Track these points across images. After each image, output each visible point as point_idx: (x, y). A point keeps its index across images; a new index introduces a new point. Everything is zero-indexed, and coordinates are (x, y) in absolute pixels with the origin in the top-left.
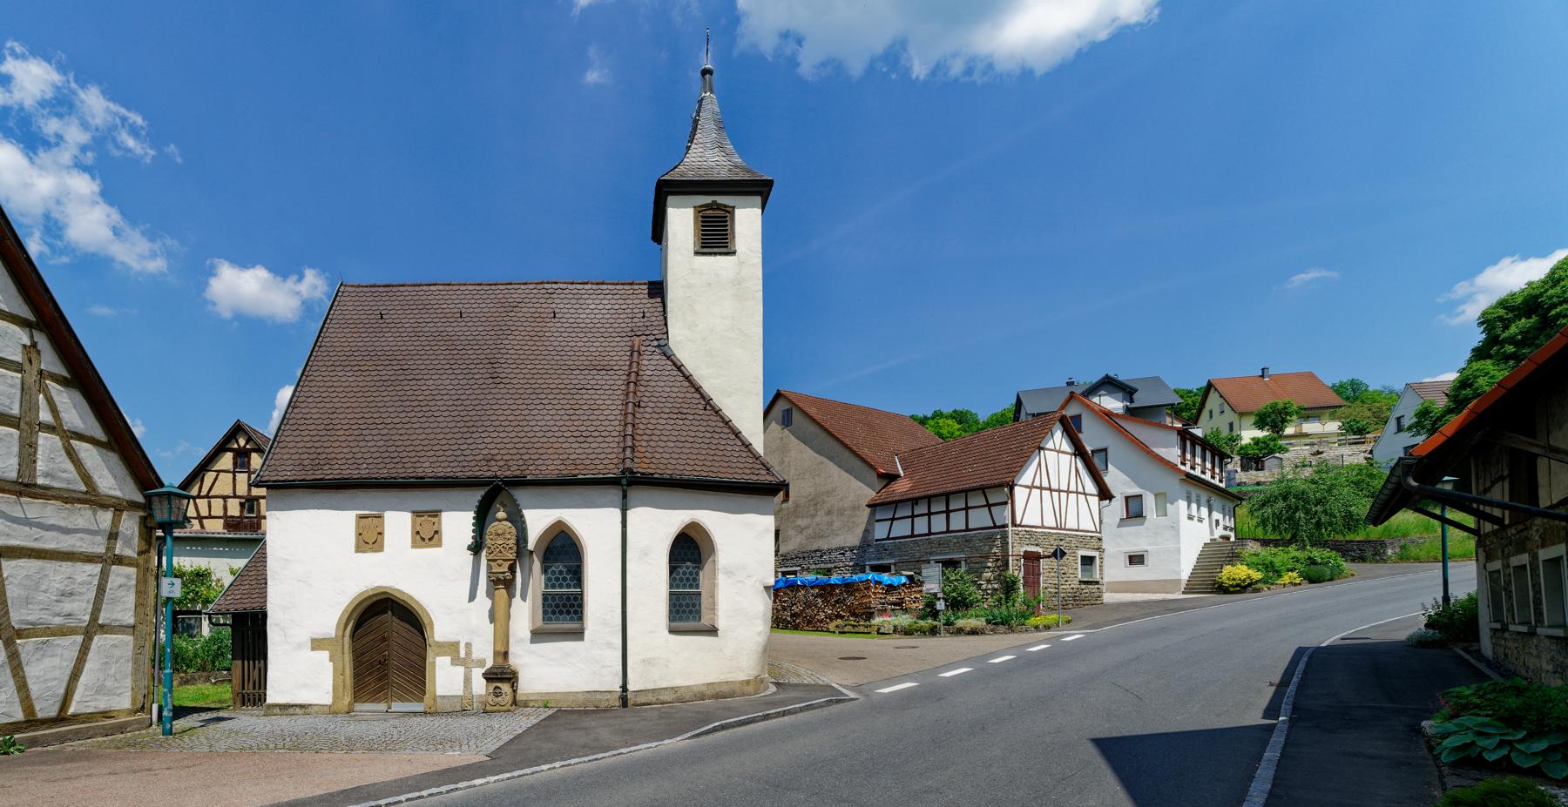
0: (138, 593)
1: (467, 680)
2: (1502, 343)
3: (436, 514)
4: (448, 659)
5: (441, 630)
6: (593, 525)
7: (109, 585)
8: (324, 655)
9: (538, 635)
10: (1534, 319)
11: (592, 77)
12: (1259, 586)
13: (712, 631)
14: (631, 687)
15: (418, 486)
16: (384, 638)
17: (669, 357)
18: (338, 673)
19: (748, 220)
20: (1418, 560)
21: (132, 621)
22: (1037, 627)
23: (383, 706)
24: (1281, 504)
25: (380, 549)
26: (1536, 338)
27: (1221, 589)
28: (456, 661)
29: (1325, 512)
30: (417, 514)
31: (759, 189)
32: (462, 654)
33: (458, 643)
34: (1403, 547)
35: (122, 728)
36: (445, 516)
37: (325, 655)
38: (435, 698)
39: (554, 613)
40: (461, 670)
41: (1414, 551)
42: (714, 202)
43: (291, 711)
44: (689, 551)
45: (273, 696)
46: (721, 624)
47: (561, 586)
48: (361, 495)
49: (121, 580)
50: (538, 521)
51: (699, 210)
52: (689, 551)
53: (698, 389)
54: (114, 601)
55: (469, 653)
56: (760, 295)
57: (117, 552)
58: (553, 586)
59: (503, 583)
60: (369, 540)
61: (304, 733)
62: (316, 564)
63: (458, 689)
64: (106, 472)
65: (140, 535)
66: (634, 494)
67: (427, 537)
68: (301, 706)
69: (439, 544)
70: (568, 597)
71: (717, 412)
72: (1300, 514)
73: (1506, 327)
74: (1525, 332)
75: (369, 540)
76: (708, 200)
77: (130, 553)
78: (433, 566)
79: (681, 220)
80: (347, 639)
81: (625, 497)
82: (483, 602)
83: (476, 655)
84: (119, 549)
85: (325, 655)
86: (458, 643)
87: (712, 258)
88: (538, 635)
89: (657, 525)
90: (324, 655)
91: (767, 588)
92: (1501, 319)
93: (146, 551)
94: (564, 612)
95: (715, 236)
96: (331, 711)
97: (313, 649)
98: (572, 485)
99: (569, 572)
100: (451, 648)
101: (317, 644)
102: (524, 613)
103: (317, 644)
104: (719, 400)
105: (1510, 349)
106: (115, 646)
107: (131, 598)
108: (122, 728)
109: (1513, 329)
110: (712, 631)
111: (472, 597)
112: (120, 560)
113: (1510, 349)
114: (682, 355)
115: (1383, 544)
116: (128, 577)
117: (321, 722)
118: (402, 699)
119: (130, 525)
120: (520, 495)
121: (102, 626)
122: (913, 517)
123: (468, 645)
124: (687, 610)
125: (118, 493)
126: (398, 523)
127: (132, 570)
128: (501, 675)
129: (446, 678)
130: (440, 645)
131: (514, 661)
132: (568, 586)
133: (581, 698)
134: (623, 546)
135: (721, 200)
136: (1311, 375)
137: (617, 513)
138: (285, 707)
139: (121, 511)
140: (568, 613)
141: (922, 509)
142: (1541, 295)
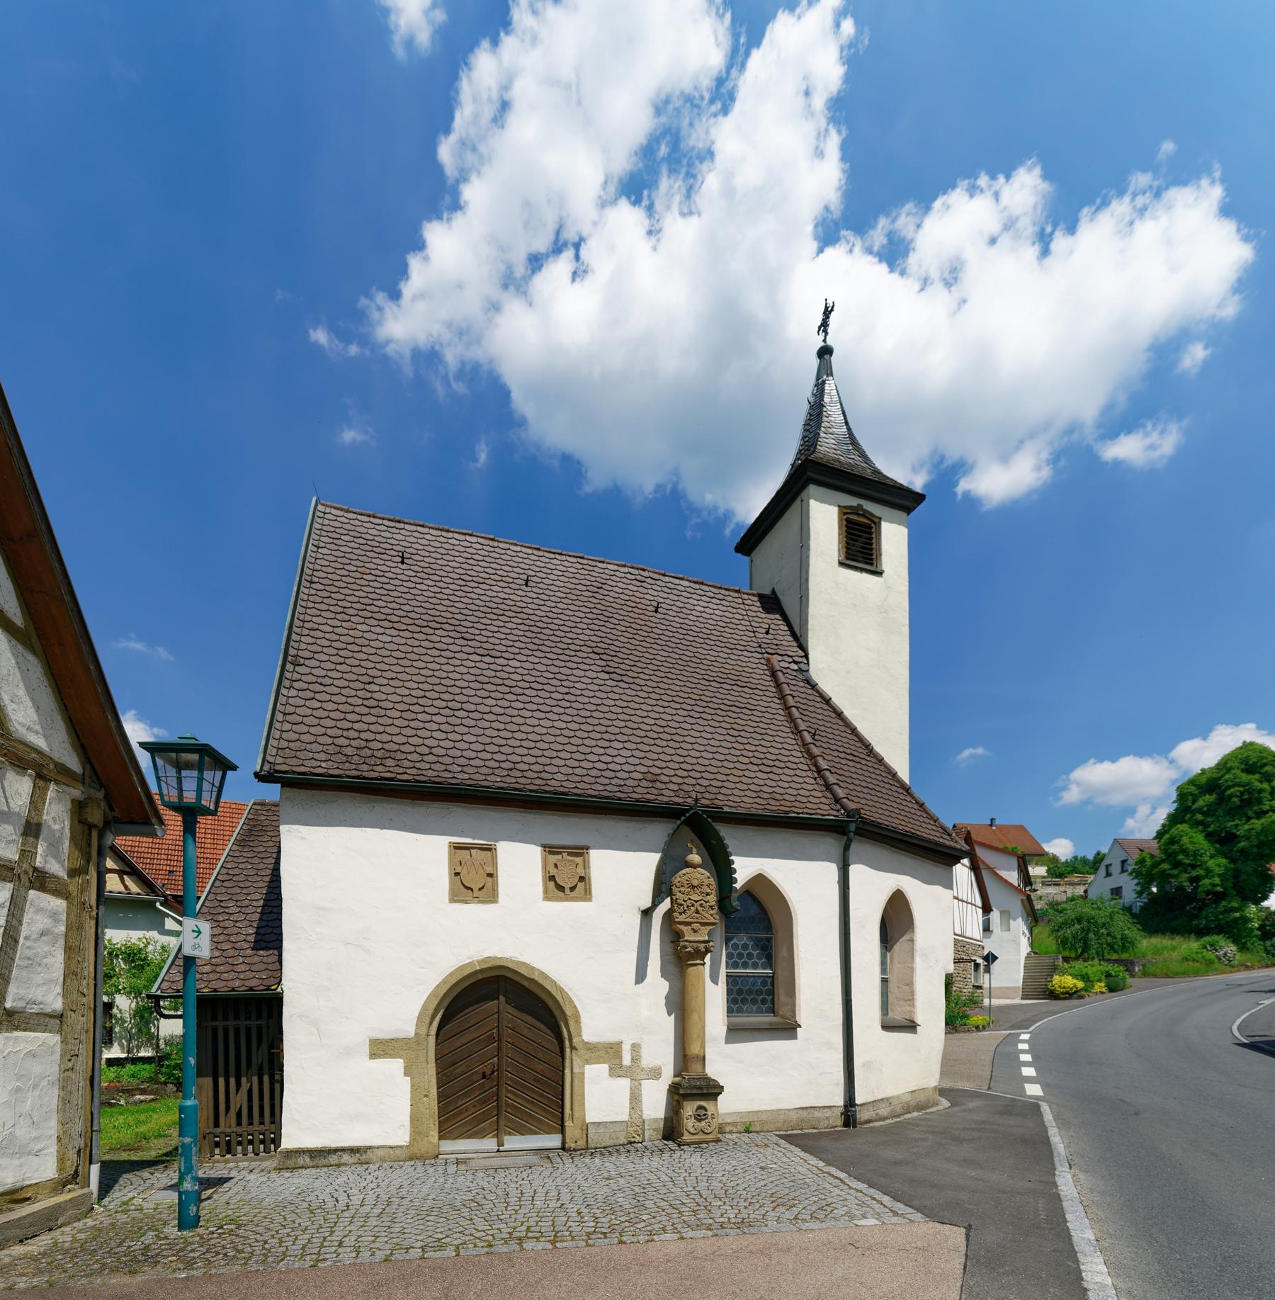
0: (68, 949)
1: (635, 1099)
2: (1194, 812)
3: (580, 851)
4: (605, 1067)
5: (592, 1024)
6: (804, 883)
7: (25, 930)
8: (396, 1065)
9: (736, 1033)
10: (1214, 796)
11: (349, 436)
12: (1083, 993)
14: (859, 1100)
15: (567, 809)
16: (497, 1043)
17: (813, 686)
18: (417, 1093)
19: (894, 538)
20: (1155, 976)
21: (58, 1005)
22: (977, 1028)
23: (489, 1144)
24: (1077, 926)
25: (493, 897)
26: (1216, 810)
27: (1052, 995)
28: (617, 1070)
29: (1109, 934)
30: (550, 849)
32: (627, 1060)
33: (619, 1044)
34: (1144, 966)
35: (48, 1221)
37: (397, 1065)
38: (585, 1128)
40: (625, 1083)
41: (1152, 969)
42: (860, 506)
43: (333, 1159)
45: (293, 1136)
47: (745, 965)
48: (458, 813)
49: (42, 922)
51: (844, 511)
52: (896, 921)
54: (32, 963)
55: (636, 1059)
56: (906, 630)
57: (39, 862)
59: (681, 958)
60: (475, 882)
62: (372, 925)
64: (21, 692)
65: (73, 838)
66: (857, 847)
67: (566, 883)
68: (353, 1151)
69: (587, 895)
70: (764, 978)
72: (1091, 935)
73: (1194, 802)
74: (1209, 806)
75: (475, 882)
77: (57, 868)
78: (587, 931)
80: (432, 1040)
81: (846, 848)
82: (658, 986)
83: (647, 1061)
84: (42, 858)
85: (397, 1065)
86: (619, 1044)
89: (873, 885)
90: (396, 1065)
92: (1191, 794)
93: (83, 871)
94: (764, 1005)
95: (860, 549)
96: (413, 1155)
97: (373, 1056)
98: (784, 825)
99: (756, 946)
100: (609, 1052)
101: (380, 1048)
102: (714, 999)
103: (380, 1048)
104: (878, 748)
105: (1200, 817)
106: (32, 1054)
107: (57, 960)
108: (48, 1221)
109: (1200, 803)
111: (640, 976)
112: (41, 881)
113: (1200, 817)
114: (826, 686)
115: (1132, 963)
116: (54, 915)
117: (400, 1177)
118: (522, 1131)
119: (57, 813)
121: (10, 1013)
123: (635, 1048)
125: (41, 743)
126: (519, 862)
127: (59, 904)
128: (693, 1088)
129: (601, 1098)
130: (591, 1047)
131: (715, 1069)
132: (755, 966)
133: (795, 1116)
135: (869, 506)
136: (1022, 828)
137: (830, 871)
138: (319, 1156)
139: (48, 780)
140: (754, 1001)
142: (1220, 778)
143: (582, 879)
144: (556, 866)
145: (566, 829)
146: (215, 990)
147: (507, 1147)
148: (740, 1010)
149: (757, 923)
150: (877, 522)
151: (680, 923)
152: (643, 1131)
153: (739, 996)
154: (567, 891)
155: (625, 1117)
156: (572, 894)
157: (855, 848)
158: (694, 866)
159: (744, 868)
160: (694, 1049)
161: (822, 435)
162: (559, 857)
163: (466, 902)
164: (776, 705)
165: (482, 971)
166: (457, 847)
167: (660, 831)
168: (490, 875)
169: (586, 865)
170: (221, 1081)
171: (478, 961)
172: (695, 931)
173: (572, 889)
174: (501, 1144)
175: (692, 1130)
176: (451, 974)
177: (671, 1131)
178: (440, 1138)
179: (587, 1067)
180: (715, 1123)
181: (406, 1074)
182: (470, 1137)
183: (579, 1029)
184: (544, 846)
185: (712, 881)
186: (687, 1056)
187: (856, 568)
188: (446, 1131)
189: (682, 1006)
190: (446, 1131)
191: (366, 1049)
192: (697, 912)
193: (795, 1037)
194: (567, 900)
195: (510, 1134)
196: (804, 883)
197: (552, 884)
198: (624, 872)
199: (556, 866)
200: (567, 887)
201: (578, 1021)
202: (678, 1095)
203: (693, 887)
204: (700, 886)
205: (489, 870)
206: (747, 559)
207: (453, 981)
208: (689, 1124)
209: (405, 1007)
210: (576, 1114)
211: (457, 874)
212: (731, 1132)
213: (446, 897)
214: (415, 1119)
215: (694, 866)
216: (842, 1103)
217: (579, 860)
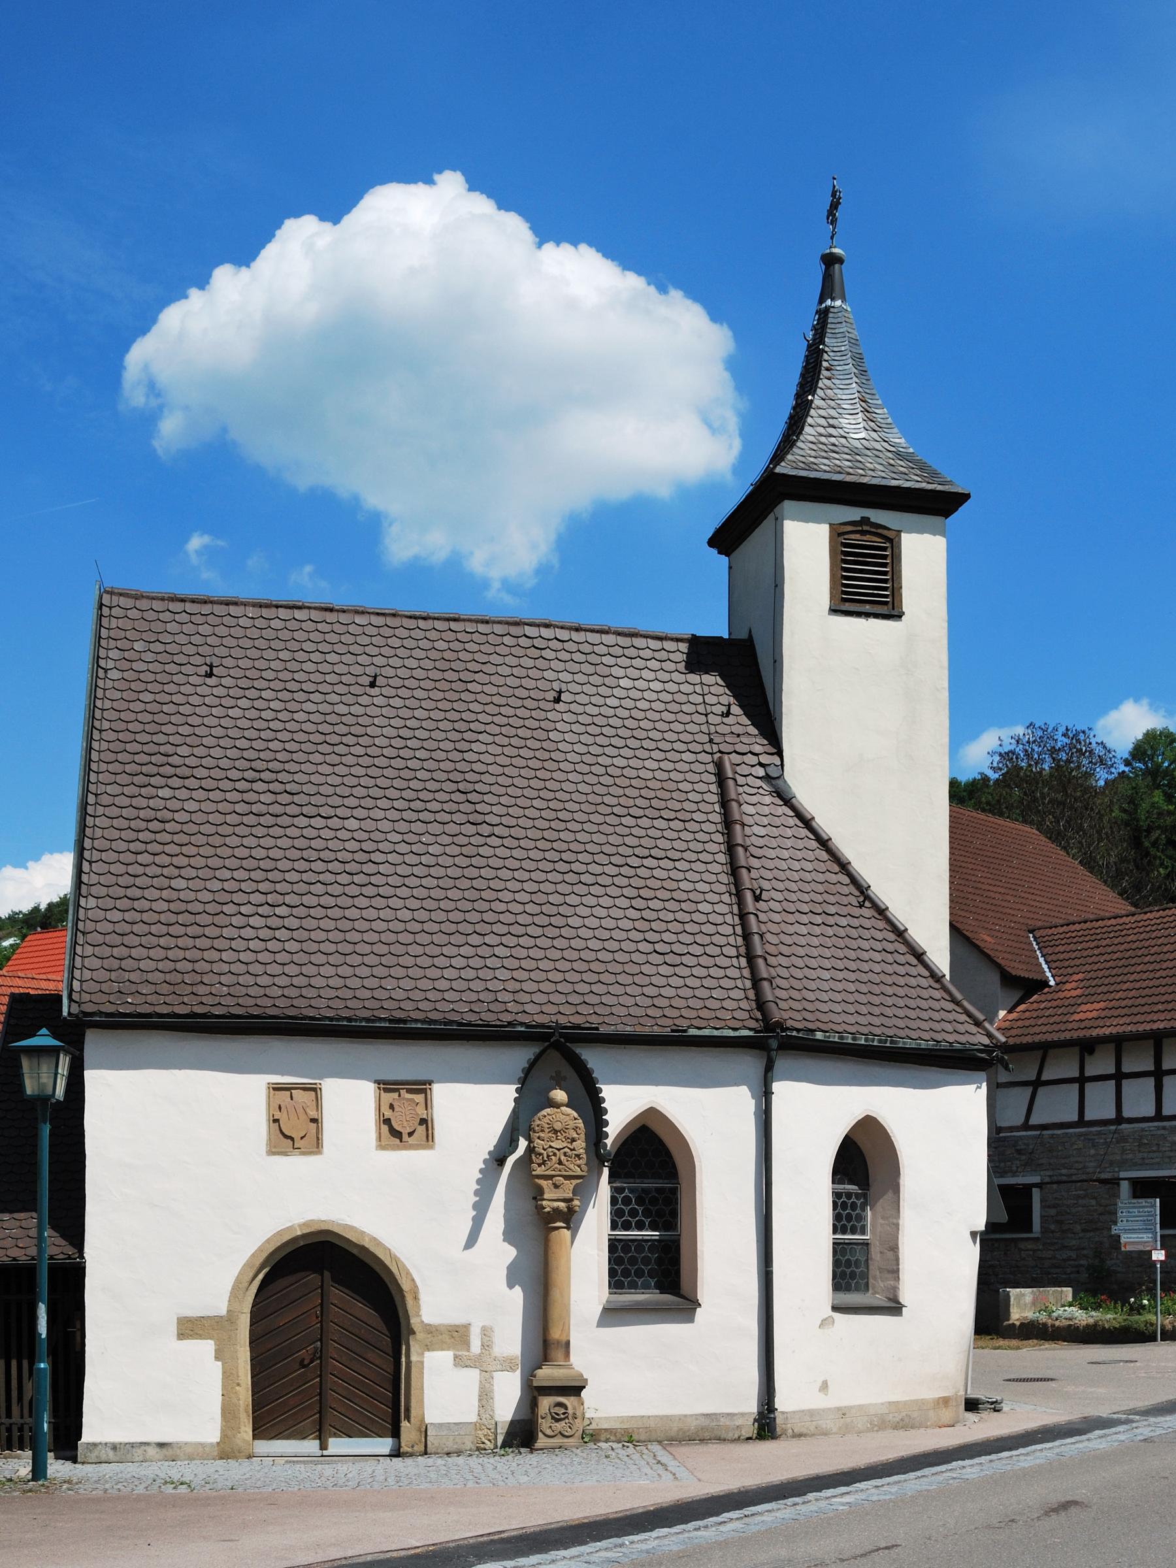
1: (485, 1396)
3: (421, 1087)
5: (431, 1306)
6: (709, 1117)
9: (612, 1315)
13: (894, 1308)
15: (404, 1034)
17: (787, 800)
18: (228, 1377)
19: (923, 555)
25: (317, 1146)
30: (386, 1086)
31: (937, 504)
32: (476, 1346)
33: (467, 1327)
36: (440, 1091)
37: (207, 1347)
39: (626, 1273)
40: (473, 1375)
42: (865, 521)
43: (138, 1453)
44: (863, 1165)
46: (905, 1297)
50: (623, 1104)
51: (837, 533)
52: (863, 1165)
53: (844, 866)
55: (486, 1346)
58: (627, 1226)
60: (295, 1130)
61: (169, 1500)
63: (467, 1413)
67: (405, 1128)
71: (881, 912)
75: (295, 1130)
76: (854, 514)
78: (422, 1182)
79: (806, 546)
82: (497, 1251)
85: (207, 1347)
86: (467, 1327)
87: (861, 621)
88: (612, 1315)
89: (816, 1112)
91: (973, 1234)
94: (655, 1271)
95: (866, 585)
97: (181, 1336)
98: (675, 1044)
99: (640, 1201)
100: (455, 1336)
101: (189, 1328)
103: (189, 1328)
110: (894, 1308)
120: (593, 1057)
122: (1082, 1080)
123: (486, 1332)
124: (862, 1276)
129: (450, 1391)
130: (431, 1330)
132: (640, 1227)
134: (752, 1148)
135: (878, 516)
138: (629, 1437)
141: (1101, 1064)
143: (423, 1121)
144: (392, 1107)
145: (404, 1060)
146: (14, 1259)
147: (331, 1450)
148: (848, 1289)
149: (652, 1171)
150: (893, 543)
151: (539, 1177)
152: (496, 1435)
153: (624, 1266)
154: (405, 1137)
155: (473, 1418)
156: (411, 1140)
157: (781, 1064)
158: (557, 1105)
159: (623, 1104)
160: (555, 1334)
161: (817, 402)
162: (396, 1095)
163: (285, 1154)
164: (717, 846)
165: (304, 1236)
166: (277, 1088)
167: (519, 1056)
168: (314, 1121)
169: (427, 1104)
170: (14, 1363)
171: (299, 1226)
172: (556, 1186)
173: (410, 1134)
174: (323, 1447)
175: (549, 1432)
176: (268, 1241)
177: (522, 1435)
178: (255, 1437)
179: (427, 1354)
180: (579, 1425)
181: (217, 1358)
182: (288, 1438)
183: (418, 1307)
184: (378, 1082)
185: (580, 1123)
186: (544, 1341)
187: (859, 614)
188: (260, 1431)
189: (540, 1281)
190: (260, 1431)
191: (173, 1329)
192: (560, 1163)
193: (691, 1320)
194: (405, 1148)
195: (335, 1435)
196: (709, 1117)
197: (385, 1128)
198: (474, 1108)
199: (392, 1107)
200: (405, 1132)
201: (416, 1298)
202: (533, 1392)
203: (556, 1132)
204: (565, 1130)
205: (313, 1114)
206: (724, 560)
207: (271, 1248)
208: (545, 1425)
209: (219, 1278)
210: (413, 1413)
211: (276, 1121)
212: (607, 1441)
213: (263, 1148)
214: (228, 1413)
215: (557, 1105)
216: (755, 1410)
217: (419, 1098)
